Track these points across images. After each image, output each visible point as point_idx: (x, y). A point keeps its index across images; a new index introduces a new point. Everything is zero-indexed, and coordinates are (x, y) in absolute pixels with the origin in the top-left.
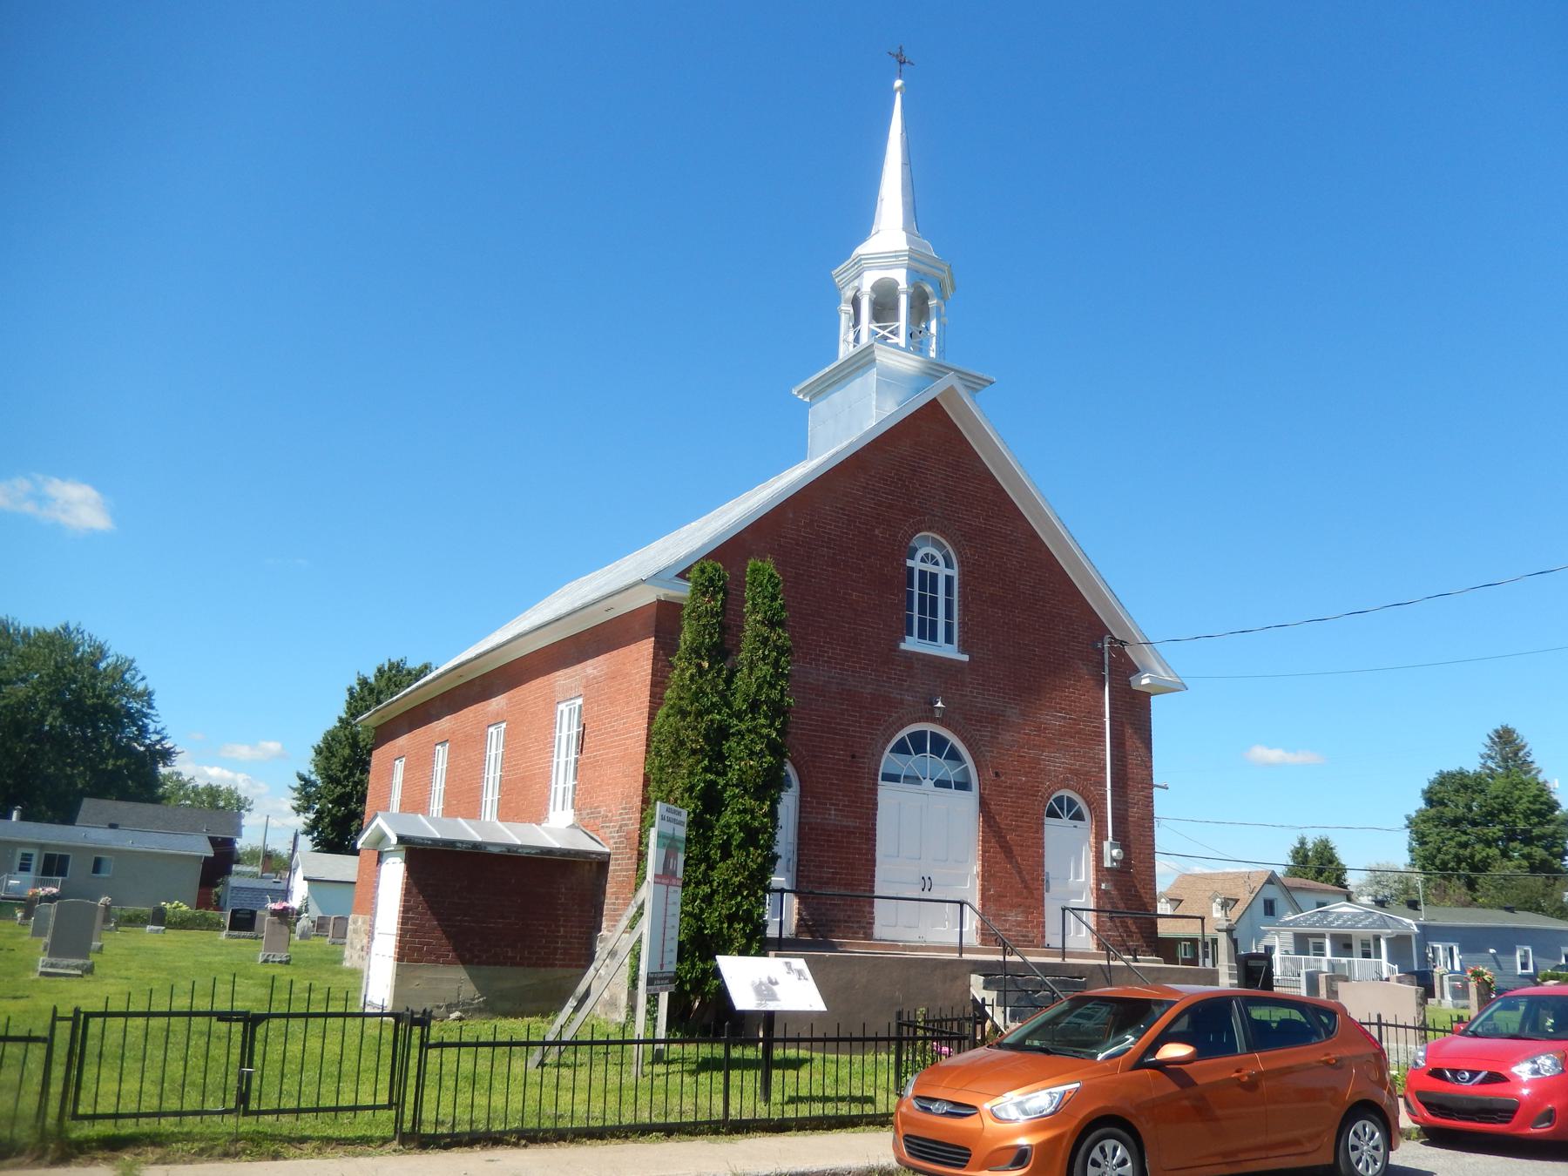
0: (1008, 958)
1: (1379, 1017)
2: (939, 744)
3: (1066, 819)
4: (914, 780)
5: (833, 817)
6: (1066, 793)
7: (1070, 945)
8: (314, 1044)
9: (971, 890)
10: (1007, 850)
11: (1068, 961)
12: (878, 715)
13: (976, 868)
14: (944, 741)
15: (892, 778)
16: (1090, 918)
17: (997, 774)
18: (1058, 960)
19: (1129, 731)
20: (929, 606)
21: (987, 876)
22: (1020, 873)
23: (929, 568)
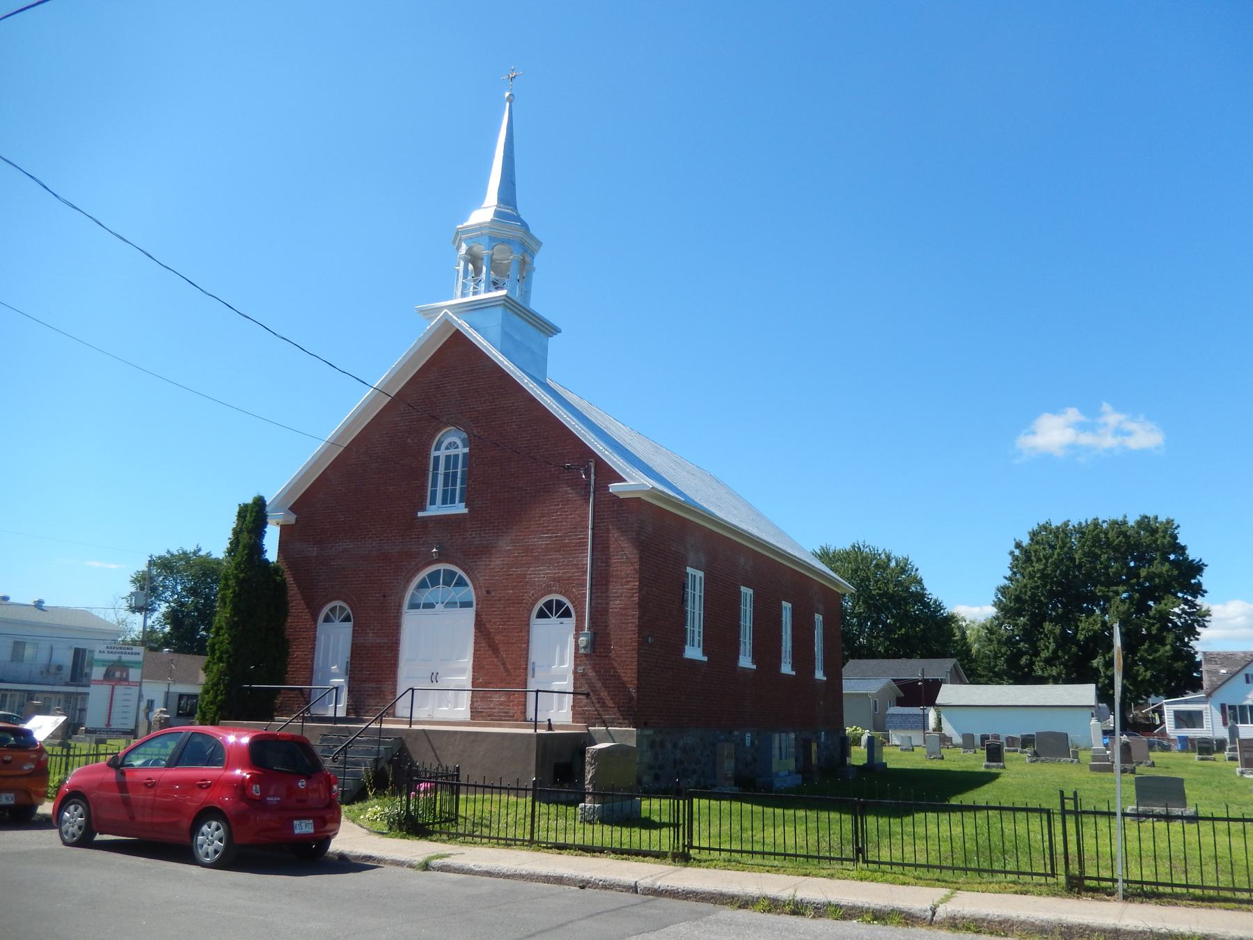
0: (384, 726)
1: (1075, 793)
2: (449, 578)
3: (337, 622)
4: (430, 606)
5: (371, 638)
6: (555, 597)
7: (416, 716)
8: (812, 839)
9: (465, 679)
10: (494, 649)
11: (414, 727)
12: (404, 566)
13: (468, 661)
14: (453, 574)
15: (414, 606)
16: (568, 700)
17: (488, 592)
18: (407, 727)
19: (614, 534)
20: (450, 478)
21: (477, 667)
22: (504, 664)
23: (452, 452)
